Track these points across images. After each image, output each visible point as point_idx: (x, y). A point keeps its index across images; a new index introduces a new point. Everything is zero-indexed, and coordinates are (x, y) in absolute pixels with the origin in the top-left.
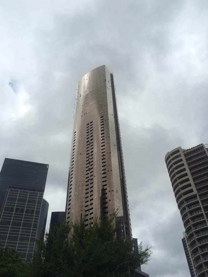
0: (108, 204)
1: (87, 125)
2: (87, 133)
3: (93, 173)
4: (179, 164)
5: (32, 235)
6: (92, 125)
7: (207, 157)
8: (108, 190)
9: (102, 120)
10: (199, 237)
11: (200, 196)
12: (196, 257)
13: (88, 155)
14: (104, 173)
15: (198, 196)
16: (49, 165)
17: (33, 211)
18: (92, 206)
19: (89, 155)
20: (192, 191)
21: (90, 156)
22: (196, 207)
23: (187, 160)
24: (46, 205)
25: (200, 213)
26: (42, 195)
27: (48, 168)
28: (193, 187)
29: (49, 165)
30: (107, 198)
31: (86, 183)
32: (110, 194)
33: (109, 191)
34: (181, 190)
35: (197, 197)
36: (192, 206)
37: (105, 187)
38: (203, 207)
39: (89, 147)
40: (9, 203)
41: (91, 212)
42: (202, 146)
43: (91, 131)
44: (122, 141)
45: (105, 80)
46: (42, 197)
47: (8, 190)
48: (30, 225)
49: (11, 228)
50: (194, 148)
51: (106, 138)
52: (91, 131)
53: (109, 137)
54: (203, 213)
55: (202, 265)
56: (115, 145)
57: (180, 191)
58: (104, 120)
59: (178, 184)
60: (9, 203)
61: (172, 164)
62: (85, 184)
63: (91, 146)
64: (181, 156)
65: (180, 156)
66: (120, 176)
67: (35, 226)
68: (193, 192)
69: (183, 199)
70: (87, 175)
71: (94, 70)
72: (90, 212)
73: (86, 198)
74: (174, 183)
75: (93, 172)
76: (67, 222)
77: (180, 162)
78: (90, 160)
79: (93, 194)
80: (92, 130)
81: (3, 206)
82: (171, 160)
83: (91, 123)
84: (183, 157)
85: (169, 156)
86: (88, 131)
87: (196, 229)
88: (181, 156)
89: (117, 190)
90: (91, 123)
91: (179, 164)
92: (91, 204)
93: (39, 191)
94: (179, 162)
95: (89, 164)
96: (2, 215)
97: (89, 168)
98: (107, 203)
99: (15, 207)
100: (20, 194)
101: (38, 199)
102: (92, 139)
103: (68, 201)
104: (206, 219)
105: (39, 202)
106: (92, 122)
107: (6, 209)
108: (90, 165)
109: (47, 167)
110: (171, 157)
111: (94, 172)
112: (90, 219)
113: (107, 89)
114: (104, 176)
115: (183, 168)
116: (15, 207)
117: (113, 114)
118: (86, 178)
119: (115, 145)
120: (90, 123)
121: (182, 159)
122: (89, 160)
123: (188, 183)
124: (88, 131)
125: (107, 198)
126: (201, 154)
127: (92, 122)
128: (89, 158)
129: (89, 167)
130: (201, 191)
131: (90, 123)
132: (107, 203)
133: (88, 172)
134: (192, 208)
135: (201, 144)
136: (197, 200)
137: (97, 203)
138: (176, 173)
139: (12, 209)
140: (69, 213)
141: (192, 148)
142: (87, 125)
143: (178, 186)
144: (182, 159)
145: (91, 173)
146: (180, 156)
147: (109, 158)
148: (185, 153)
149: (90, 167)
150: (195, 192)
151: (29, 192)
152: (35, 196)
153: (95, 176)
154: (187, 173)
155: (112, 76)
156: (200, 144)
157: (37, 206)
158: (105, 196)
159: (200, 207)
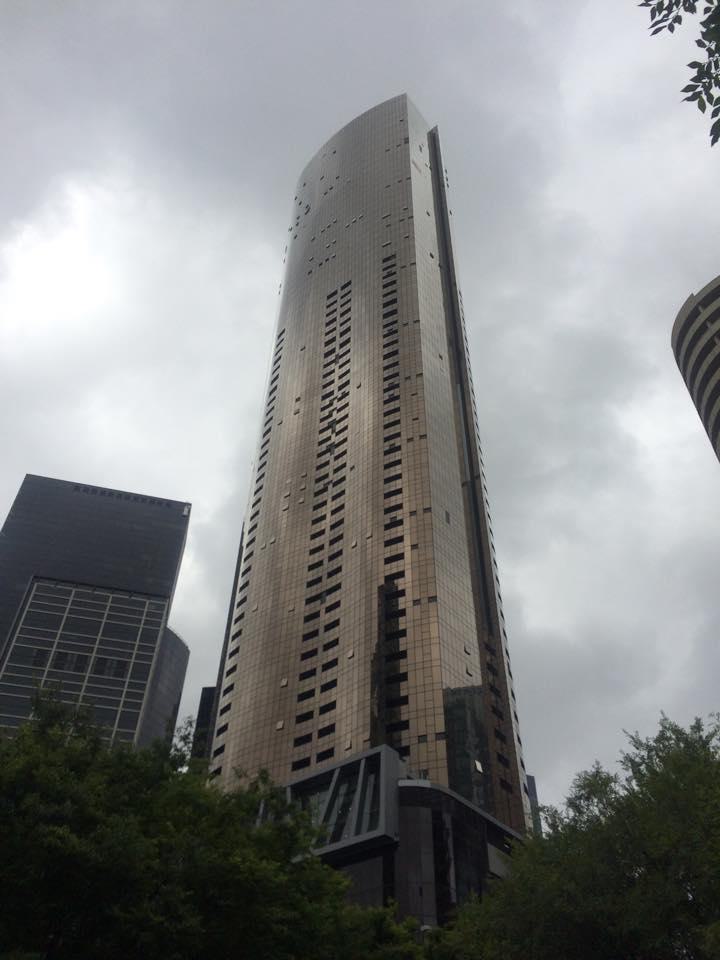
8: (409, 596)
9: (391, 381)
13: (322, 483)
17: (123, 666)
19: (321, 592)
21: (330, 486)
30: (405, 725)
31: (312, 557)
32: (417, 616)
33: (416, 602)
39: (327, 463)
40: (30, 632)
44: (478, 413)
45: (407, 141)
47: (33, 584)
51: (413, 513)
53: (418, 321)
56: (441, 357)
57: (699, 313)
58: (404, 437)
60: (30, 632)
61: (703, 320)
63: (336, 458)
66: (463, 472)
69: (699, 304)
72: (328, 604)
75: (337, 605)
76: (215, 747)
78: (336, 416)
80: (339, 569)
81: (23, 609)
89: (447, 515)
93: (148, 595)
95: (330, 430)
97: (329, 443)
98: (404, 595)
103: (244, 544)
106: (349, 283)
107: (19, 655)
108: (333, 432)
109: (185, 513)
113: (412, 165)
117: (436, 254)
118: (318, 481)
119: (441, 357)
122: (331, 404)
124: (317, 542)
125: (405, 725)
128: (332, 408)
129: (329, 438)
132: (404, 595)
133: (316, 606)
137: (356, 680)
139: (43, 655)
140: (230, 688)
145: (329, 609)
147: (417, 419)
149: (335, 439)
151: (111, 596)
155: (433, 138)
158: (397, 605)
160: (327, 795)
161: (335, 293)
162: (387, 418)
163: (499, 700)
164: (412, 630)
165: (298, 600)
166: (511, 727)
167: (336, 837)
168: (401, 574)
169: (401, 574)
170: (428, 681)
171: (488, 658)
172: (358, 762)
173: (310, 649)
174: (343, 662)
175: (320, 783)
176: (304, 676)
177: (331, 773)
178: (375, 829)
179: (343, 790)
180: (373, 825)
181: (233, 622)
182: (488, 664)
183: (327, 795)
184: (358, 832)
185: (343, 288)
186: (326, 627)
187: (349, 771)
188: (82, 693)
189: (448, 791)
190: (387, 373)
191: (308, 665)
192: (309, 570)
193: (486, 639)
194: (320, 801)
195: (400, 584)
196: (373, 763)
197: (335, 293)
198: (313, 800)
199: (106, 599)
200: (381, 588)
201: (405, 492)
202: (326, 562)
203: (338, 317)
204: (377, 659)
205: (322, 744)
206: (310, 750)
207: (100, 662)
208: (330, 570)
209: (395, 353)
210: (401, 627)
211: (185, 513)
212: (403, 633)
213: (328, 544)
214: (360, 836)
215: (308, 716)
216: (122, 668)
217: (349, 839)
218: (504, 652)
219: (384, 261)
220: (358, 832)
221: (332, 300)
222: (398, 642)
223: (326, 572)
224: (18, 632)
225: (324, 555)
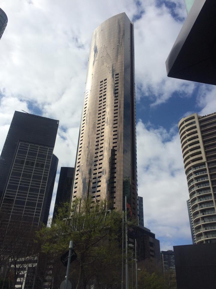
0: (117, 165)
1: (101, 82)
3: (103, 144)
4: (192, 131)
5: (39, 201)
6: (106, 91)
10: (200, 195)
11: (208, 164)
12: (192, 199)
15: (206, 164)
16: (59, 121)
18: (104, 120)
19: (98, 148)
20: (201, 158)
22: (206, 187)
23: (201, 127)
24: (55, 160)
25: (206, 180)
26: (52, 150)
27: (58, 125)
28: (203, 155)
29: (59, 121)
35: (205, 165)
36: (207, 213)
37: (115, 148)
41: (99, 190)
43: (104, 89)
46: (52, 152)
48: (34, 204)
49: (18, 192)
50: (210, 115)
52: (104, 89)
54: (207, 174)
55: (200, 219)
57: (184, 123)
59: (185, 131)
64: (195, 123)
67: (39, 205)
68: (202, 160)
69: (189, 150)
70: (99, 128)
71: (110, 19)
74: (186, 161)
77: (194, 129)
79: (101, 181)
81: (11, 171)
83: (105, 80)
86: (101, 89)
87: (199, 194)
88: (195, 123)
90: (105, 80)
91: (192, 131)
92: (104, 95)
93: (49, 146)
94: (193, 129)
96: (8, 182)
98: (115, 203)
99: (26, 160)
100: (24, 169)
101: (48, 154)
102: (105, 98)
104: (215, 206)
105: (49, 157)
106: (106, 79)
111: (106, 115)
112: (99, 168)
114: (115, 138)
115: (195, 135)
116: (24, 165)
120: (104, 81)
121: (195, 121)
123: (199, 151)
124: (101, 89)
127: (106, 79)
130: (208, 148)
131: (104, 81)
134: (200, 181)
136: (209, 186)
138: (192, 166)
141: (208, 115)
142: (101, 82)
143: (185, 133)
150: (204, 160)
152: (45, 151)
153: (107, 105)
154: (200, 146)
157: (40, 195)
162: (114, 125)
170: (120, 167)
174: (105, 128)
188: (27, 198)
199: (38, 147)
200: (112, 150)
201: (119, 80)
202: (103, 90)
204: (109, 180)
207: (37, 164)
211: (58, 123)
212: (115, 182)
215: (101, 113)
216: (42, 166)
224: (12, 170)
225: (103, 91)
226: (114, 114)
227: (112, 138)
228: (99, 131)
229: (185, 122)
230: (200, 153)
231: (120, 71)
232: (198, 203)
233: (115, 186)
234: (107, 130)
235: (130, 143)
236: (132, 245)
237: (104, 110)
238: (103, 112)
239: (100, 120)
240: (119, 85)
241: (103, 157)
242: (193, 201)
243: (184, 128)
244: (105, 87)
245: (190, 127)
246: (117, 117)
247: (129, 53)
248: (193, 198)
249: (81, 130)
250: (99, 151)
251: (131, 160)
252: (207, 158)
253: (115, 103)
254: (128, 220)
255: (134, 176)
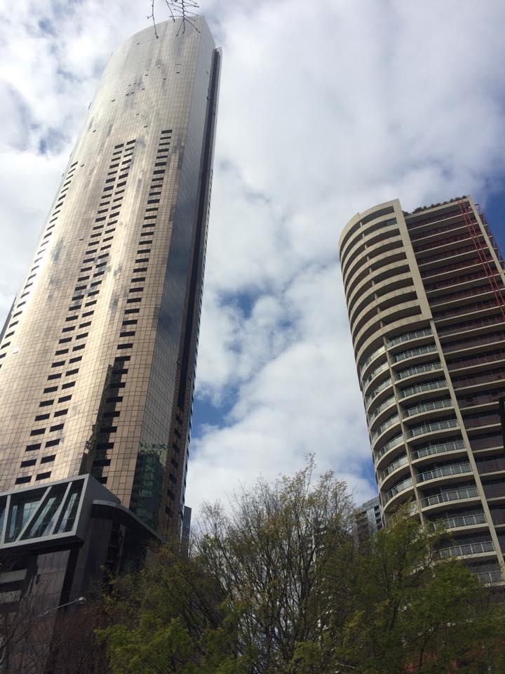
2: (108, 181)
3: (72, 388)
7: (500, 282)
8: (112, 467)
14: (135, 650)
15: (433, 325)
20: (417, 311)
25: (433, 370)
28: (422, 301)
34: (368, 259)
35: (462, 438)
38: (481, 478)
42: (465, 200)
57: (369, 273)
62: (44, 383)
65: (393, 221)
68: (416, 300)
73: (34, 433)
82: (361, 234)
84: (402, 226)
85: (359, 223)
98: (109, 465)
104: (497, 552)
110: (363, 228)
121: (398, 230)
126: (486, 286)
135: (464, 197)
136: (431, 336)
141: (433, 206)
143: (371, 286)
144: (398, 230)
146: (393, 221)
148: (408, 217)
150: (426, 314)
156: (461, 196)
159: (473, 476)
160: (38, 504)
161: (122, 145)
162: (129, 304)
163: (172, 502)
164: (127, 398)
165: (30, 415)
166: (183, 459)
167: (40, 533)
168: (128, 358)
169: (128, 358)
170: (126, 461)
171: (178, 412)
172: (68, 483)
173: (48, 399)
175: (34, 495)
176: (39, 418)
177: (45, 489)
178: (70, 530)
179: (52, 501)
180: (69, 528)
181: (8, 327)
182: (175, 430)
183: (38, 504)
184: (56, 532)
185: (128, 143)
186: (71, 360)
187: (58, 489)
189: (128, 512)
190: (139, 257)
191: (53, 383)
192: (63, 332)
193: (178, 412)
194: (31, 508)
195: (126, 365)
196: (77, 485)
197: (122, 145)
198: (27, 506)
201: (147, 280)
203: (115, 186)
205: (39, 468)
206: (32, 471)
208: (73, 357)
209: (163, 172)
210: (111, 441)
213: (76, 328)
214: (56, 535)
217: (49, 536)
218: (183, 481)
219: (163, 132)
220: (56, 532)
221: (118, 150)
222: (118, 390)
223: (66, 371)
226: (157, 165)
227: (117, 344)
228: (62, 367)
229: (364, 224)
230: (403, 256)
231: (175, 125)
232: (408, 443)
233: (122, 381)
234: (120, 250)
235: (173, 355)
236: (165, 459)
237: (74, 366)
238: (45, 460)
239: (59, 376)
240: (165, 176)
241: (133, 157)
242: (392, 487)
243: (368, 286)
244: (84, 330)
245: (397, 310)
246: (129, 350)
247: (196, 183)
248: (394, 498)
249: (13, 313)
250: (62, 384)
251: (175, 398)
252: (435, 313)
253: (126, 323)
254: (150, 455)
255: (179, 399)
